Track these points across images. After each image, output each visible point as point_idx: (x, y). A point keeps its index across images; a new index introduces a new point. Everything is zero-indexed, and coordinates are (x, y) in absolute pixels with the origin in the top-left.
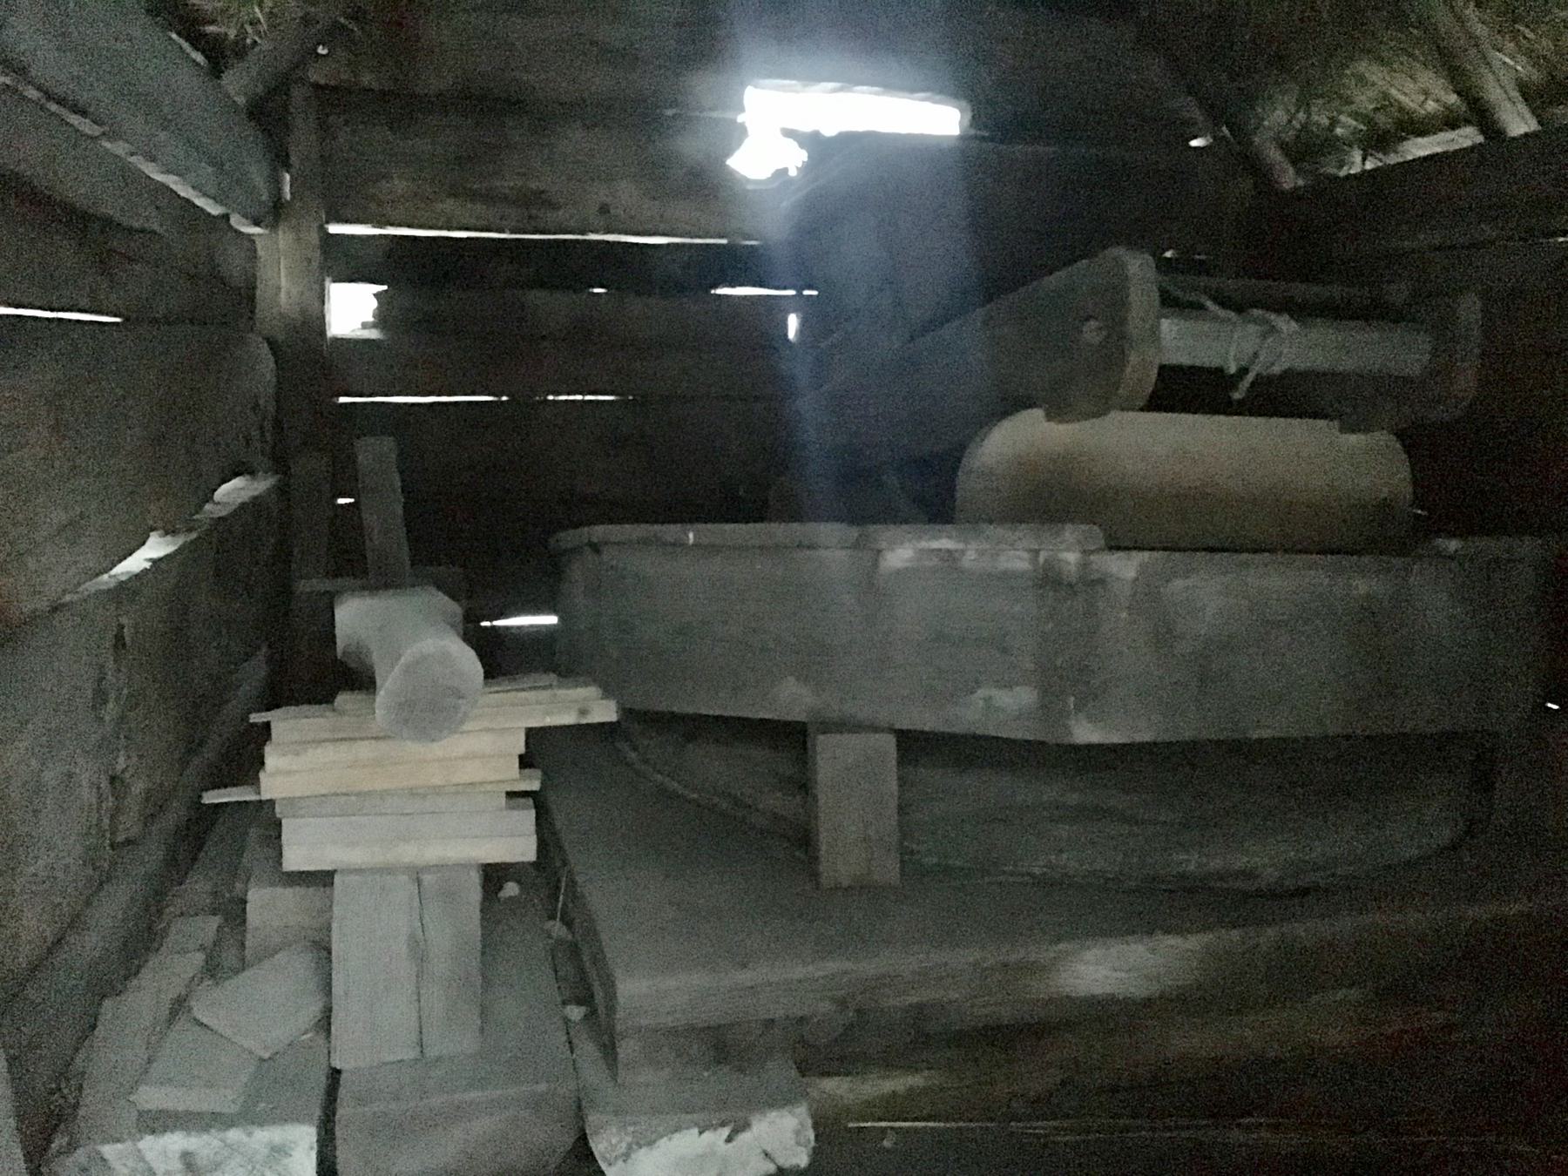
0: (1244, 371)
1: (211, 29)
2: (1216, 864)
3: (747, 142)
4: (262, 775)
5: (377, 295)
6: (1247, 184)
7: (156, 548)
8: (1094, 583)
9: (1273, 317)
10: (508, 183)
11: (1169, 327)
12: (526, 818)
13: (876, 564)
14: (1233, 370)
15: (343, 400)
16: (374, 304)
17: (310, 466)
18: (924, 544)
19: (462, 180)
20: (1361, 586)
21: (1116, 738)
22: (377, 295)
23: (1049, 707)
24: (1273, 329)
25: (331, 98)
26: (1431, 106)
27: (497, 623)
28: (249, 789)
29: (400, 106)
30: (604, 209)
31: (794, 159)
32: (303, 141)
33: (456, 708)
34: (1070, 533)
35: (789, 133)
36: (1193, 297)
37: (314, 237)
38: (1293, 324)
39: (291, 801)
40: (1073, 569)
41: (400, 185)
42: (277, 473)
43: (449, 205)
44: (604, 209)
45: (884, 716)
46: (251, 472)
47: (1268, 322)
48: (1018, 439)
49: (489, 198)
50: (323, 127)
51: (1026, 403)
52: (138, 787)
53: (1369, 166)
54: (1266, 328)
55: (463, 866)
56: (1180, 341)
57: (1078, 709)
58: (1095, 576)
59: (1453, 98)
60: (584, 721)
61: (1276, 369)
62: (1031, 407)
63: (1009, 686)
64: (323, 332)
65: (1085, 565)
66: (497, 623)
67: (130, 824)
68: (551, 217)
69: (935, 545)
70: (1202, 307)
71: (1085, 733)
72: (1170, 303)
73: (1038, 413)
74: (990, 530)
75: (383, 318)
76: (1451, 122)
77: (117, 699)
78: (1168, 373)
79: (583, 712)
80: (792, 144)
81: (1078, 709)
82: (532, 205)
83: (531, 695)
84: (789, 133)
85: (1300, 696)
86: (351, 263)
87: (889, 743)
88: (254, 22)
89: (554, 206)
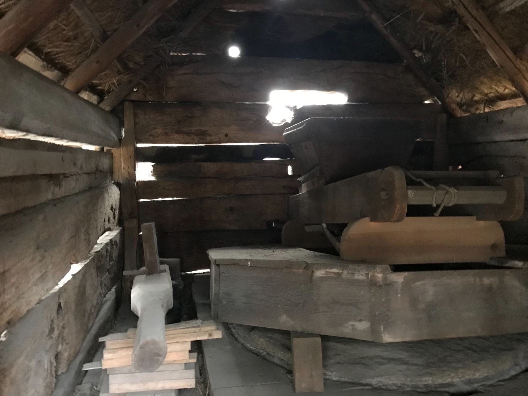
0: (438, 206)
1: (100, 88)
2: (440, 381)
3: (272, 110)
4: (102, 360)
5: (153, 166)
6: (444, 116)
7: (76, 268)
8: (389, 285)
9: (448, 188)
10: (194, 129)
11: (411, 193)
12: (192, 373)
13: (312, 275)
14: (435, 205)
15: (142, 200)
16: (152, 168)
17: (132, 224)
18: (328, 270)
19: (178, 130)
20: (486, 281)
21: (398, 340)
22: (153, 166)
23: (374, 330)
24: (447, 192)
25: (138, 104)
26: (507, 91)
27: (193, 272)
28: (97, 363)
29: (160, 106)
30: (226, 135)
31: (289, 117)
32: (129, 120)
33: (158, 360)
34: (379, 268)
35: (288, 107)
36: (419, 180)
37: (132, 149)
38: (455, 190)
39: (112, 369)
40: (380, 279)
41: (159, 131)
42: (120, 226)
43: (176, 136)
44: (226, 135)
45: (317, 331)
46: (109, 229)
47: (446, 189)
48: (362, 228)
49: (189, 134)
50: (135, 115)
51: (363, 216)
52: (66, 355)
53: (487, 110)
54: (445, 192)
55: (170, 390)
56: (415, 196)
57: (384, 331)
58: (388, 282)
59: (514, 89)
60: (211, 338)
61: (451, 204)
62: (365, 217)
63: (360, 320)
64: (135, 180)
65: (385, 279)
66: (193, 272)
67: (63, 368)
68: (209, 138)
69: (332, 270)
70: (423, 185)
71: (387, 338)
72: (411, 183)
73: (367, 219)
74: (351, 266)
75: (155, 172)
76: (514, 96)
77: (58, 329)
78: (410, 207)
79: (210, 335)
80: (288, 110)
81: (384, 331)
82: (201, 135)
83: (192, 330)
84: (288, 107)
85: (467, 321)
86: (143, 156)
87: (319, 339)
88: (113, 84)
89: (210, 135)
